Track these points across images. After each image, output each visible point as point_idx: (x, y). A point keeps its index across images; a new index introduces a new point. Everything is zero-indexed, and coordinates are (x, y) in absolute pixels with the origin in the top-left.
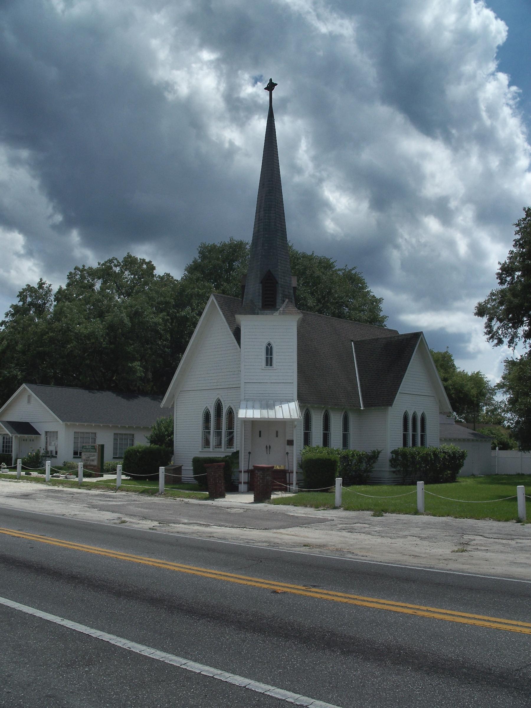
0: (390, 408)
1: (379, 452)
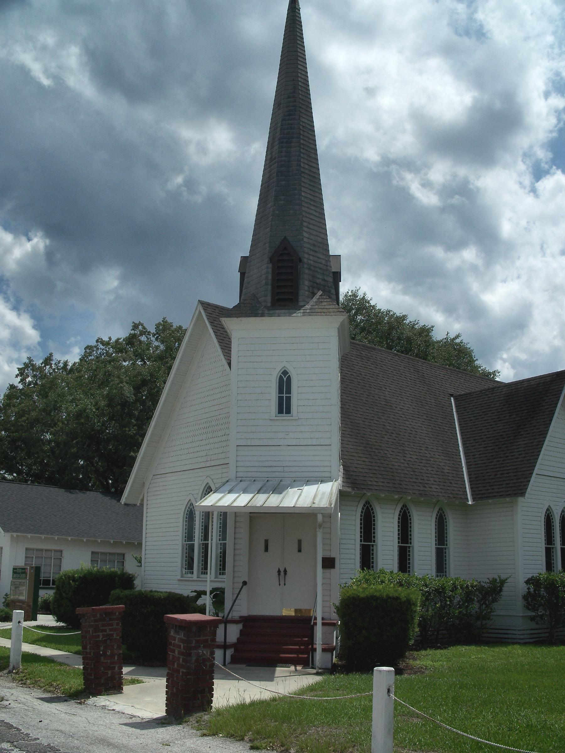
0: (520, 499)
1: (503, 582)
